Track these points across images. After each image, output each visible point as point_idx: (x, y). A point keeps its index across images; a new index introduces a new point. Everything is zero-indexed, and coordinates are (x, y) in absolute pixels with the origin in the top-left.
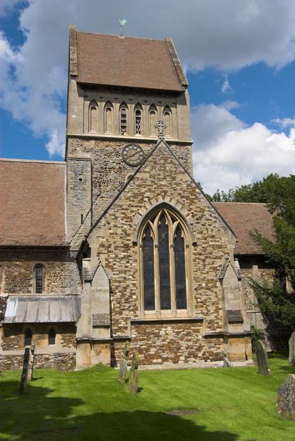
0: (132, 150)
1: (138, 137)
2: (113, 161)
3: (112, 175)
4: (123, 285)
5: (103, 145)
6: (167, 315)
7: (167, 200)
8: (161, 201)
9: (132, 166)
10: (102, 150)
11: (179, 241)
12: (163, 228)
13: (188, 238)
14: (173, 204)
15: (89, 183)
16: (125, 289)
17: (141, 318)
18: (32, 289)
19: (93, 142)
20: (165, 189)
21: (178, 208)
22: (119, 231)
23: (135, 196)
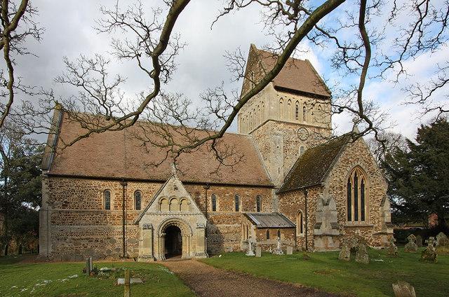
0: (303, 131)
1: (305, 123)
2: (293, 138)
3: (292, 146)
4: (340, 208)
5: (287, 127)
6: (356, 223)
7: (359, 163)
8: (356, 164)
9: (377, 133)
10: (287, 130)
11: (363, 186)
12: (356, 179)
13: (367, 184)
14: (361, 165)
15: (282, 150)
16: (341, 210)
17: (347, 225)
18: (256, 209)
19: (282, 124)
20: (358, 157)
21: (364, 168)
22: (338, 180)
23: (345, 160)
